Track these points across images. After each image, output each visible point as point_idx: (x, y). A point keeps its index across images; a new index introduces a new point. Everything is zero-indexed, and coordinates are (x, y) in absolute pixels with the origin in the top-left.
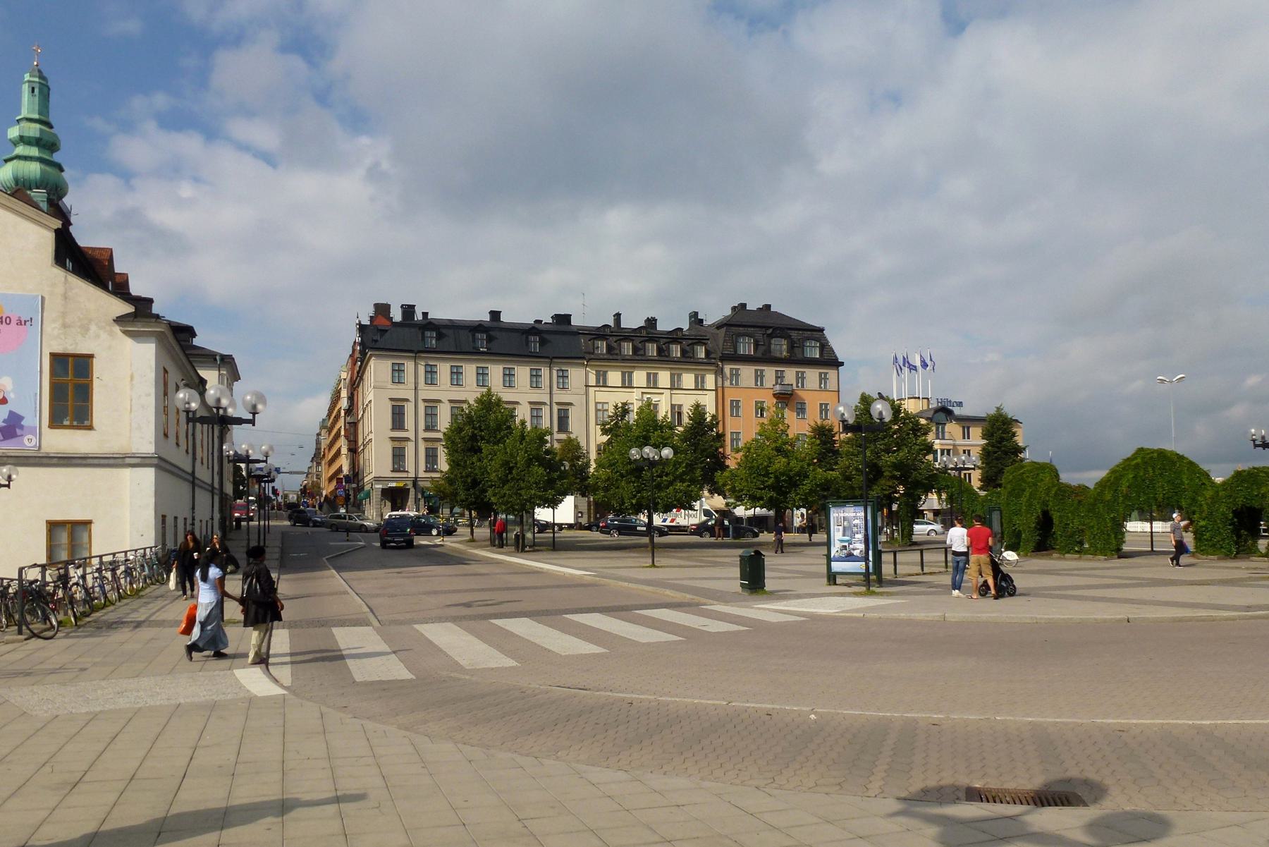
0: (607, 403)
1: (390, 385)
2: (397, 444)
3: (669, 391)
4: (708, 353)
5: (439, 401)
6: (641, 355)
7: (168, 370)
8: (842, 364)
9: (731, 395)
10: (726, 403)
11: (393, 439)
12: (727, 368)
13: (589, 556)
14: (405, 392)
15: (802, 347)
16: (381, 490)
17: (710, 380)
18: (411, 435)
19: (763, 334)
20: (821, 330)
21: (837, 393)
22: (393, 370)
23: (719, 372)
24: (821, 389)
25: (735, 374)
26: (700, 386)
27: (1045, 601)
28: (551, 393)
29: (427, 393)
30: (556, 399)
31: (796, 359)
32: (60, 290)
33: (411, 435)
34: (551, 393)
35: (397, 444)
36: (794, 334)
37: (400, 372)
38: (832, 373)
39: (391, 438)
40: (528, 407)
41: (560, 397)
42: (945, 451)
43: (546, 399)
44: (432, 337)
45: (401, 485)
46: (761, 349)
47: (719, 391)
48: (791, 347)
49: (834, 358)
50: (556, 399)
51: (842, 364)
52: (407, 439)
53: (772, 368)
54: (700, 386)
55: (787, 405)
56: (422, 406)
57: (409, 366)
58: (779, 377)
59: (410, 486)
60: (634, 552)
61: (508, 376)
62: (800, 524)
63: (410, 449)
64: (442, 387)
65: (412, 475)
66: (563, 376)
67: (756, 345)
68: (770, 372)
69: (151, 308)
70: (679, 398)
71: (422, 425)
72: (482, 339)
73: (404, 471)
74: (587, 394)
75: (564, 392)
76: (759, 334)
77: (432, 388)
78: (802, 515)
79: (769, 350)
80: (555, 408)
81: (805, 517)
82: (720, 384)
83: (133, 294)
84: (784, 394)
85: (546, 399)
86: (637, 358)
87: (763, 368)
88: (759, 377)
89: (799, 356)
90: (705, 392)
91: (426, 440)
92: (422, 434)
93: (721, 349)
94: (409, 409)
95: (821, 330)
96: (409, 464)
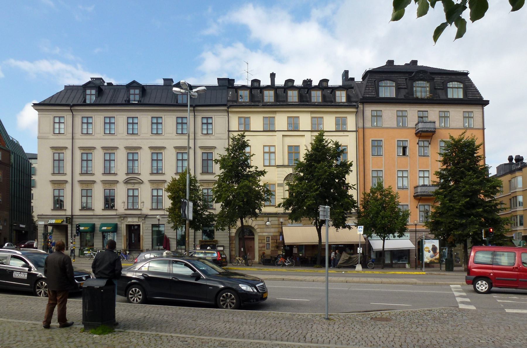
0: (274, 146)
2: (108, 187)
3: (310, 133)
4: (348, 97)
5: (94, 148)
6: (283, 101)
8: (487, 103)
9: (371, 135)
10: (366, 143)
11: (53, 182)
12: (369, 110)
15: (445, 89)
16: (43, 226)
18: (68, 178)
19: (406, 79)
20: (466, 74)
21: (482, 131)
22: (177, 123)
24: (398, 127)
25: (377, 116)
27: (168, 308)
29: (82, 142)
30: (199, 143)
33: (68, 178)
36: (438, 79)
37: (183, 125)
38: (476, 111)
39: (51, 181)
40: (174, 152)
43: (68, 143)
44: (91, 95)
46: (403, 93)
48: (433, 90)
49: (478, 98)
50: (199, 143)
51: (487, 103)
52: (66, 182)
53: (459, 109)
54: (341, 128)
55: (430, 144)
56: (78, 154)
60: (496, 295)
62: (431, 259)
66: (207, 123)
67: (398, 89)
69: (417, 64)
71: (78, 170)
72: (91, 95)
73: (137, 209)
75: (208, 137)
76: (402, 80)
78: (434, 249)
79: (412, 92)
81: (438, 251)
82: (361, 125)
84: (427, 131)
85: (68, 143)
86: (303, 103)
87: (404, 109)
88: (402, 117)
89: (443, 97)
90: (346, 133)
93: (363, 93)
95: (466, 74)
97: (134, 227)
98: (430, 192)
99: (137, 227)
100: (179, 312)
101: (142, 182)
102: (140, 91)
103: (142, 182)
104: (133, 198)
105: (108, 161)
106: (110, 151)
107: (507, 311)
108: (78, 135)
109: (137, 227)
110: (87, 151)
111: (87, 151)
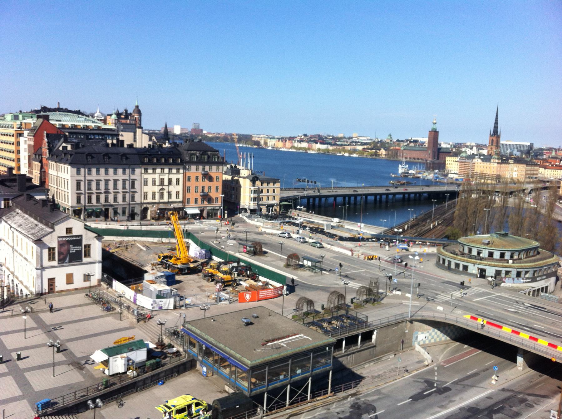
1: (76, 175)
7: (256, 319)
11: (77, 193)
13: (541, 347)
14: (81, 178)
17: (181, 171)
18: (83, 192)
23: (184, 168)
26: (178, 172)
28: (85, 176)
31: (210, 162)
32: (85, 233)
33: (83, 192)
34: (85, 176)
35: (79, 195)
41: (133, 177)
42: (157, 183)
43: (83, 178)
45: (80, 208)
47: (184, 174)
52: (82, 193)
57: (82, 170)
58: (204, 169)
59: (83, 208)
61: (210, 169)
63: (82, 197)
64: (94, 175)
65: (83, 205)
68: (201, 167)
70: (171, 176)
74: (141, 176)
77: (79, 176)
80: (131, 181)
83: (97, 351)
85: (83, 178)
91: (88, 193)
92: (87, 191)
94: (82, 184)
96: (82, 201)
97: (320, 200)
98: (454, 244)
99: (413, 195)
100: (555, 173)
101: (111, 193)
102: (207, 165)
103: (111, 193)
104: (106, 199)
105: (115, 187)
106: (98, 182)
107: (425, 393)
108: (87, 175)
109: (413, 195)
110: (90, 181)
111: (90, 181)
